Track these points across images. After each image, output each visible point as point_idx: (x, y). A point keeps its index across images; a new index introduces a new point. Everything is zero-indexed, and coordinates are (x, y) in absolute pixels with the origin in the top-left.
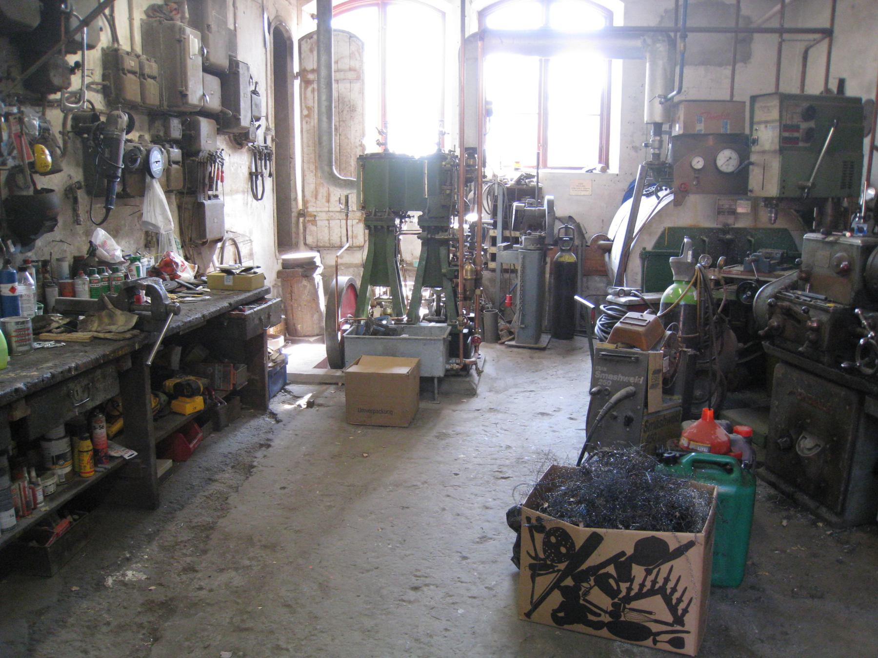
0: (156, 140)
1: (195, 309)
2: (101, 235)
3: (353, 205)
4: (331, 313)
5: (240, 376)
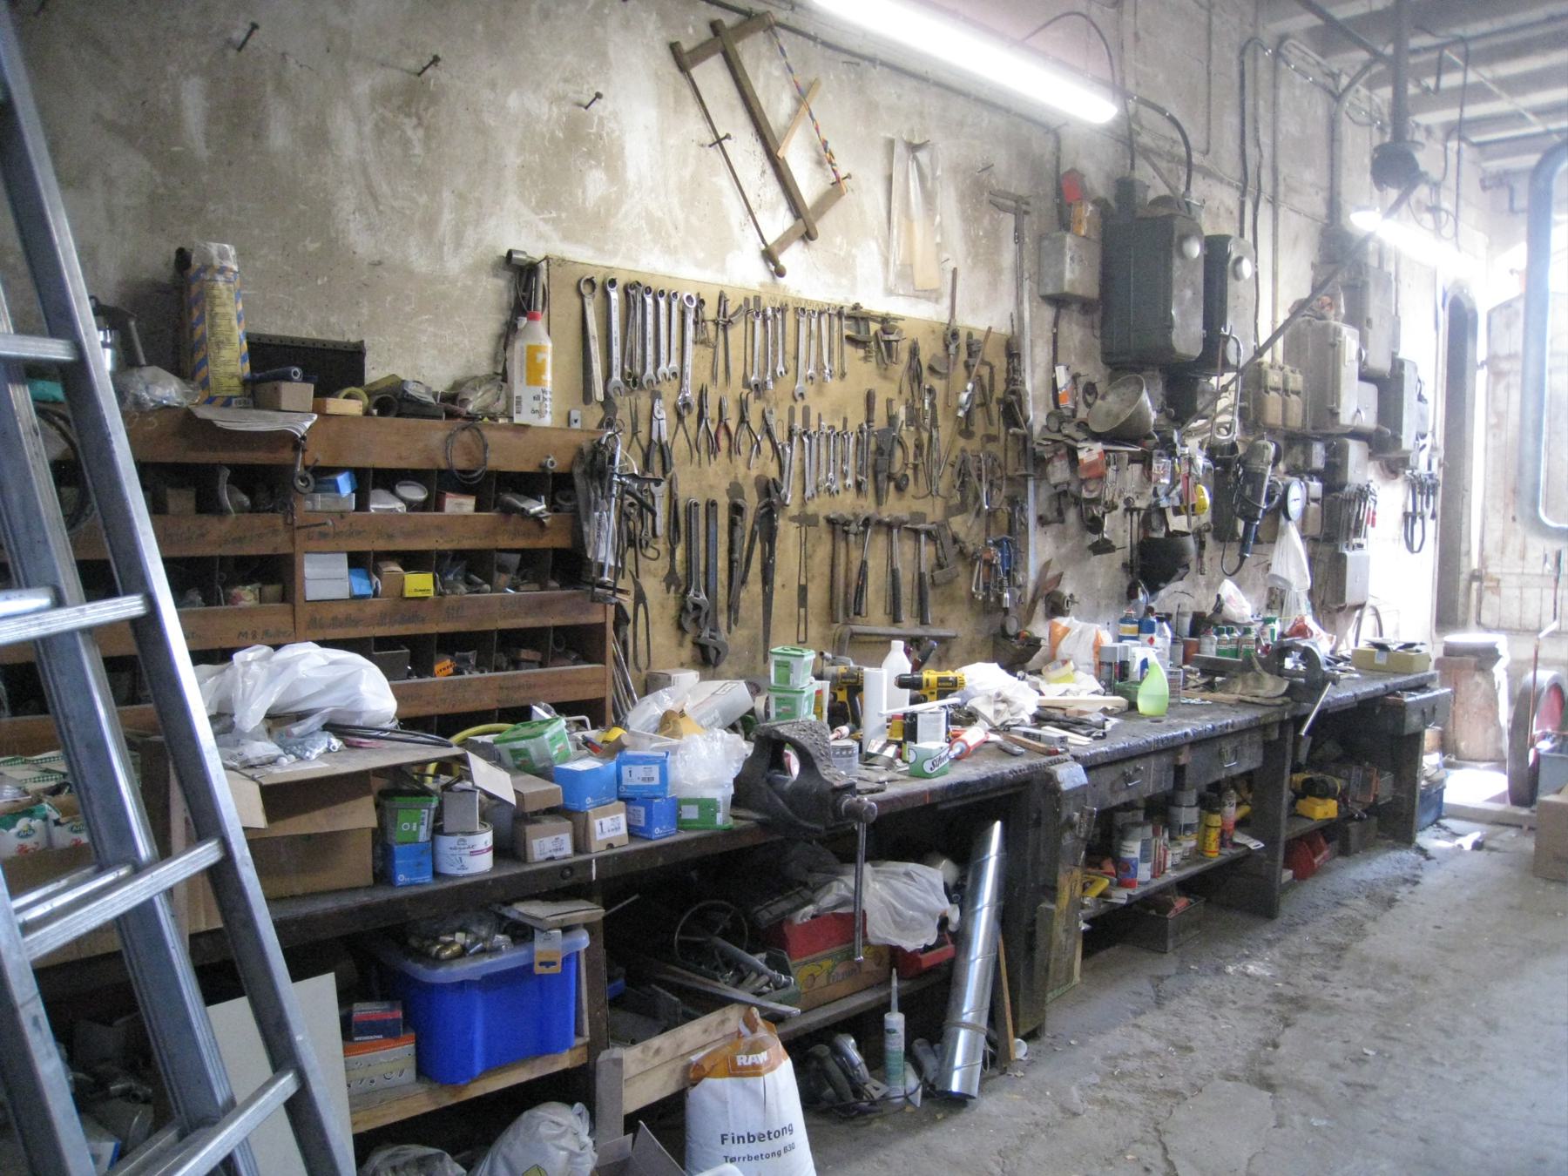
0: (1293, 471)
1: (1347, 689)
2: (1228, 588)
4: (1520, 725)
5: (1384, 786)
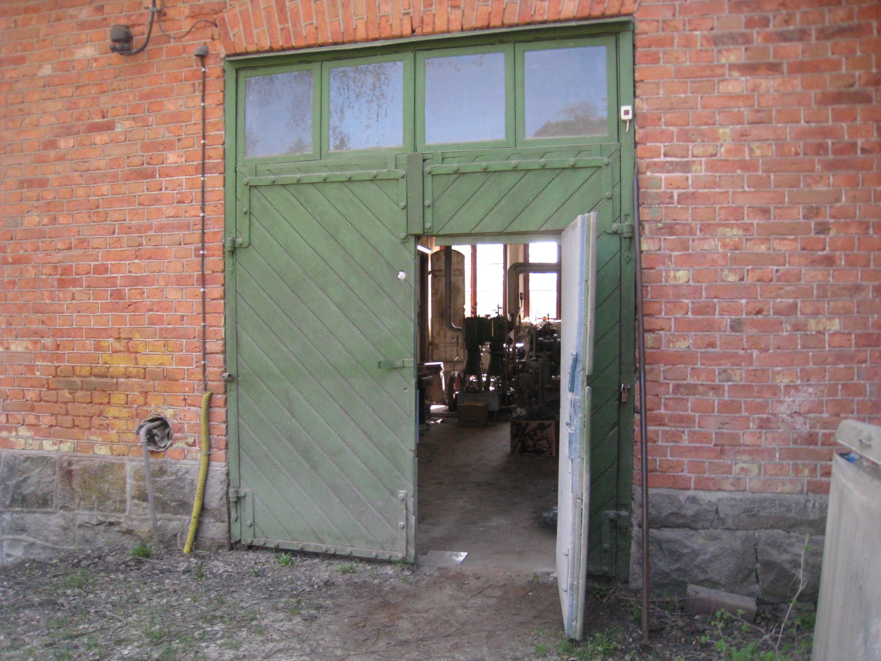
3: (460, 341)
